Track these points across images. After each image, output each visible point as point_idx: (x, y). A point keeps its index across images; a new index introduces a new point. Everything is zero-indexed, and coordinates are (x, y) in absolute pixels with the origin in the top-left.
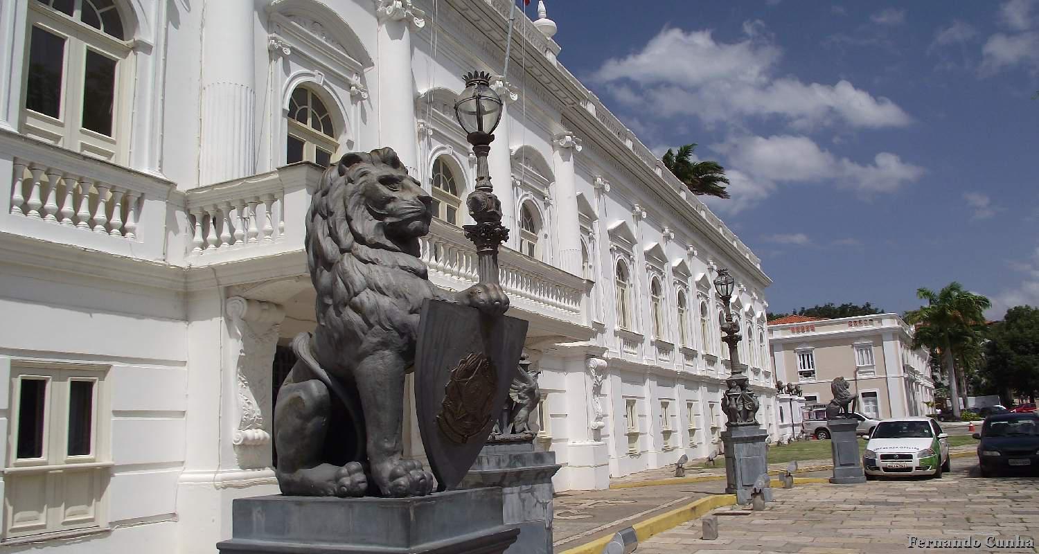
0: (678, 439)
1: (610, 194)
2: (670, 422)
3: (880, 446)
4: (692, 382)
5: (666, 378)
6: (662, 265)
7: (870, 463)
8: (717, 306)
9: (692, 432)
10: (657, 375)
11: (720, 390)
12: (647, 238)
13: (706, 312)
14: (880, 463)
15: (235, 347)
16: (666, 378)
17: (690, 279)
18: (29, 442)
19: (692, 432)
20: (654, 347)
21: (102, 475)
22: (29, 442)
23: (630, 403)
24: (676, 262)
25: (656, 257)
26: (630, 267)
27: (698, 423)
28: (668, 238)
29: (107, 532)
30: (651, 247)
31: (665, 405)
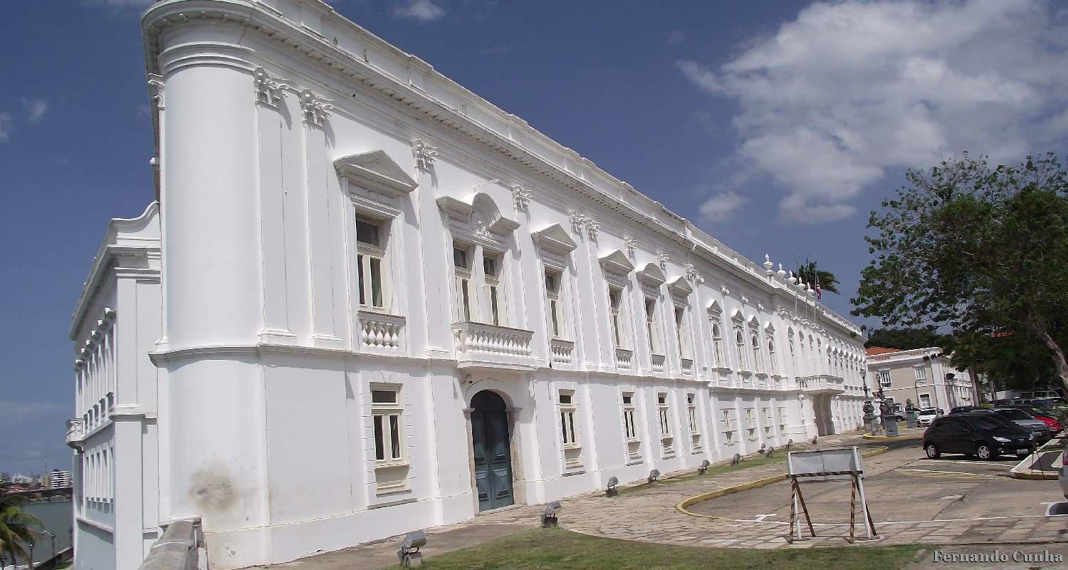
0: (759, 433)
1: (764, 311)
2: (730, 425)
3: (921, 418)
4: (853, 398)
5: (747, 395)
6: (741, 322)
7: (919, 422)
8: (734, 328)
9: (767, 429)
10: (718, 393)
11: (756, 399)
12: (731, 308)
13: (719, 333)
14: (921, 422)
15: (812, 404)
16: (765, 395)
17: (744, 323)
18: (380, 455)
19: (767, 429)
20: (717, 373)
21: (403, 470)
22: (380, 455)
23: (780, 409)
24: (750, 319)
25: (738, 319)
26: (742, 334)
27: (755, 423)
28: (725, 294)
29: (733, 444)
30: (606, 256)
31: (749, 411)
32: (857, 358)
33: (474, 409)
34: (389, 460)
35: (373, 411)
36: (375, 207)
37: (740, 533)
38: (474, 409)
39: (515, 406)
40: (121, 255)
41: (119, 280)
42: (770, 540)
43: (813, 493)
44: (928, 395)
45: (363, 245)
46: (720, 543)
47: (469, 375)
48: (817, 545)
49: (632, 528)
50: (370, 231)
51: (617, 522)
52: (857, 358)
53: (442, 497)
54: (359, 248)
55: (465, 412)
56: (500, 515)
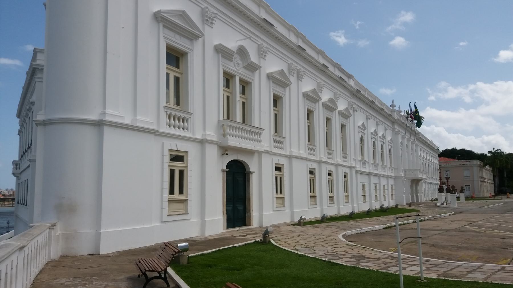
18: (172, 192)
32: (424, 157)
33: (228, 170)
34: (279, 195)
35: (169, 166)
36: (180, 43)
37: (384, 260)
38: (228, 170)
39: (251, 170)
40: (38, 68)
41: (37, 83)
42: (407, 268)
43: (339, 234)
44: (469, 185)
45: (169, 67)
46: (373, 266)
47: (226, 150)
48: (445, 274)
49: (315, 249)
50: (175, 58)
51: (336, 247)
52: (424, 157)
53: (205, 220)
54: (167, 68)
55: (223, 171)
56: (237, 231)
